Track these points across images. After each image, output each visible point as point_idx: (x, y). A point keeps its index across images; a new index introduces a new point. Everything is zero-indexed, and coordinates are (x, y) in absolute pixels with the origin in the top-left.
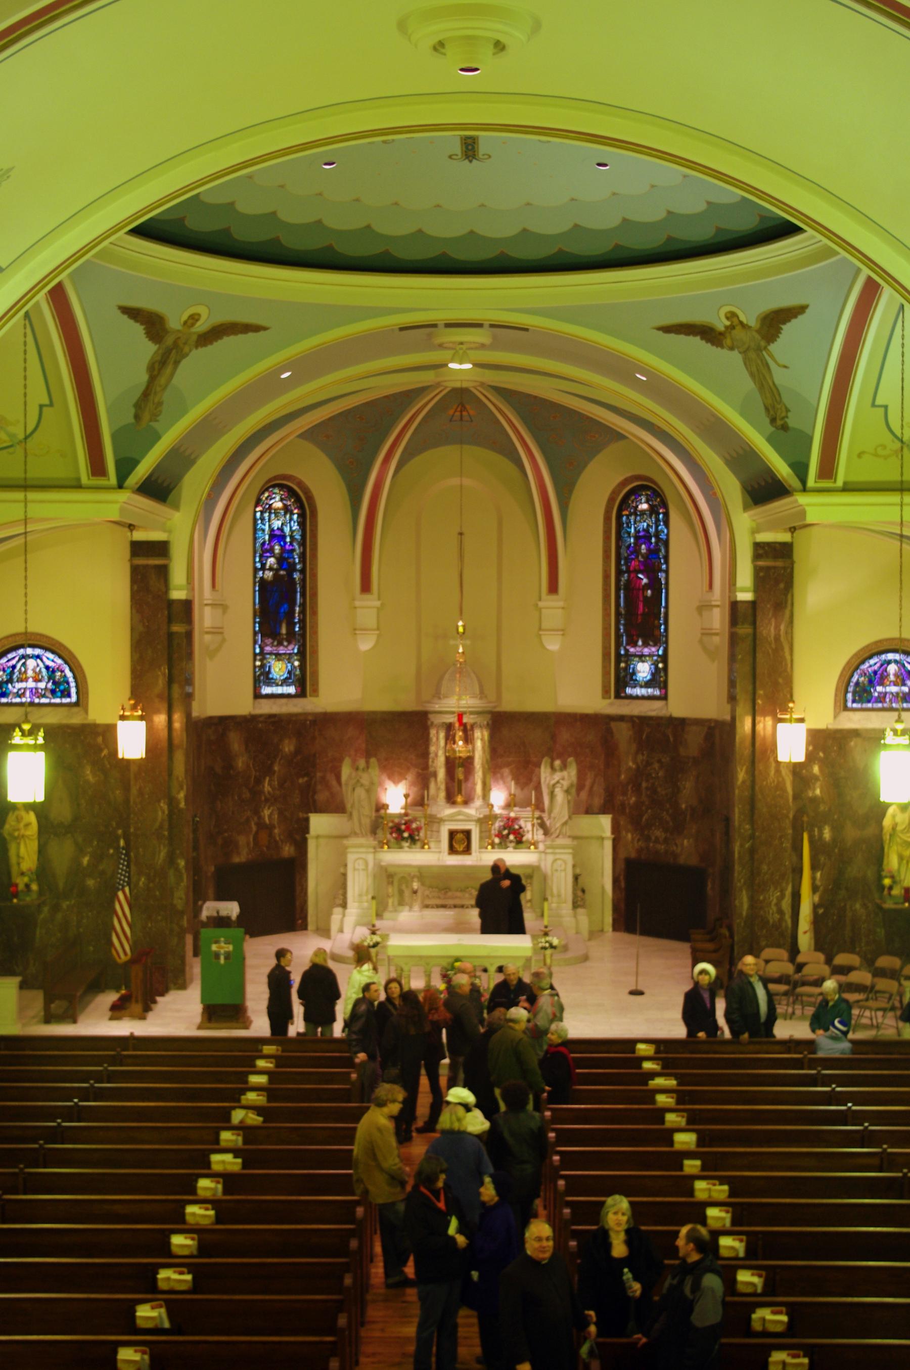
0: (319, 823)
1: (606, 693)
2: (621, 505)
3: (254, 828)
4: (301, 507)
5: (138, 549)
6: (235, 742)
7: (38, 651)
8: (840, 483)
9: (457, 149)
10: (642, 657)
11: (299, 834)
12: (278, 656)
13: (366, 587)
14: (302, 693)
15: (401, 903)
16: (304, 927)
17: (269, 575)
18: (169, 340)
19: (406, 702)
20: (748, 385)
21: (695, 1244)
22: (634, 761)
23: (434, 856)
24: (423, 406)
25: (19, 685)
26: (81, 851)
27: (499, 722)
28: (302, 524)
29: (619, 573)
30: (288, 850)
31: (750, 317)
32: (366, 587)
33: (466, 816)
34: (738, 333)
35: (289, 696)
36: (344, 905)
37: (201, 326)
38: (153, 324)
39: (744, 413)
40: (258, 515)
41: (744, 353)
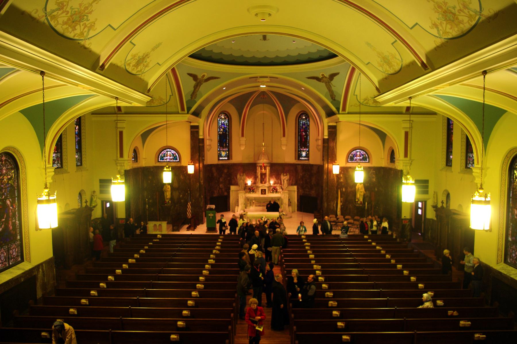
0: (233, 188)
1: (296, 159)
2: (299, 117)
4: (228, 118)
5: (192, 127)
6: (214, 170)
8: (347, 112)
9: (262, 38)
10: (303, 151)
11: (228, 190)
12: (223, 151)
13: (243, 136)
14: (228, 159)
15: (251, 205)
18: (198, 81)
19: (251, 161)
20: (326, 90)
23: (258, 195)
24: (255, 95)
26: (180, 194)
27: (273, 166)
28: (228, 122)
29: (299, 132)
30: (226, 194)
31: (327, 75)
32: (243, 136)
33: (265, 186)
34: (324, 79)
35: (226, 160)
36: (238, 206)
37: (205, 78)
38: (194, 77)
39: (326, 97)
41: (326, 83)
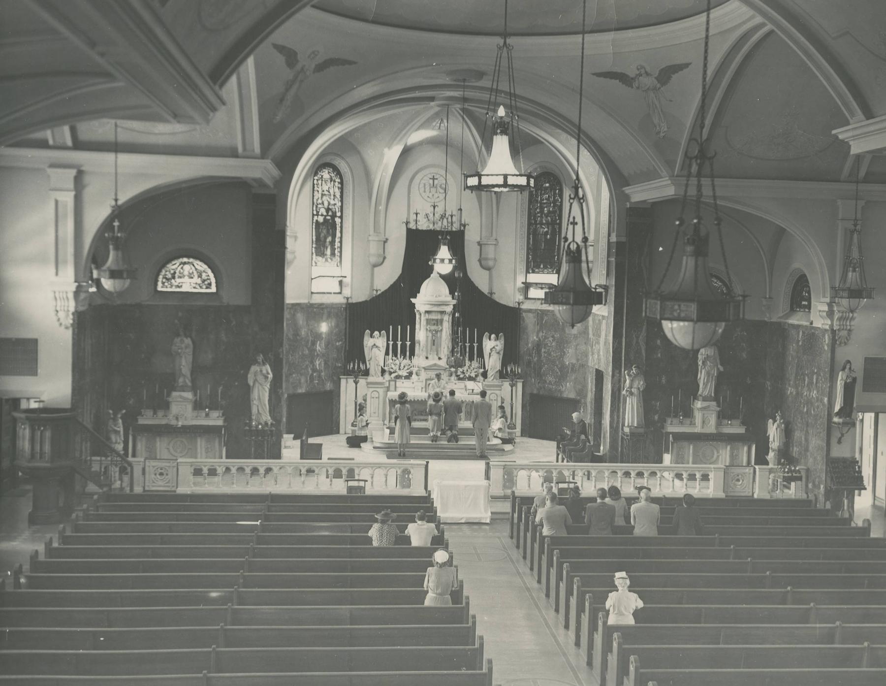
3: (310, 372)
7: (191, 260)
16: (338, 433)
17: (321, 219)
21: (846, 519)
22: (537, 337)
25: (178, 280)
30: (329, 386)
40: (315, 182)
